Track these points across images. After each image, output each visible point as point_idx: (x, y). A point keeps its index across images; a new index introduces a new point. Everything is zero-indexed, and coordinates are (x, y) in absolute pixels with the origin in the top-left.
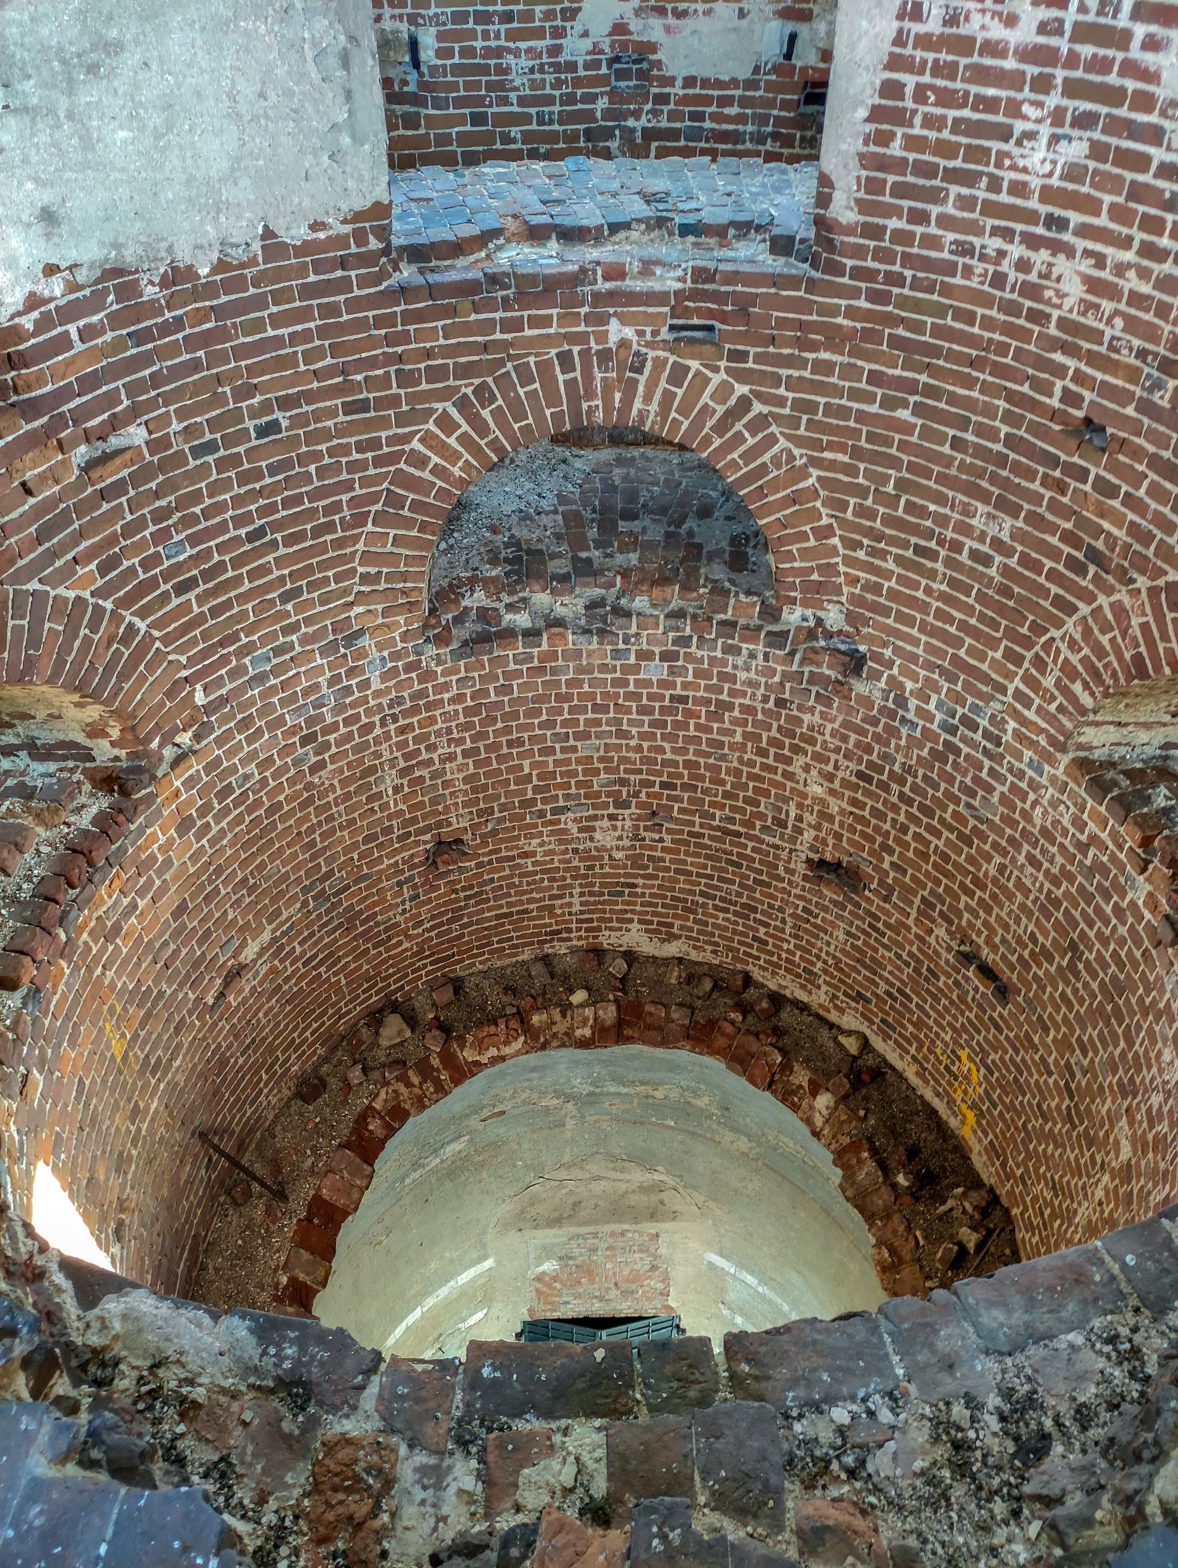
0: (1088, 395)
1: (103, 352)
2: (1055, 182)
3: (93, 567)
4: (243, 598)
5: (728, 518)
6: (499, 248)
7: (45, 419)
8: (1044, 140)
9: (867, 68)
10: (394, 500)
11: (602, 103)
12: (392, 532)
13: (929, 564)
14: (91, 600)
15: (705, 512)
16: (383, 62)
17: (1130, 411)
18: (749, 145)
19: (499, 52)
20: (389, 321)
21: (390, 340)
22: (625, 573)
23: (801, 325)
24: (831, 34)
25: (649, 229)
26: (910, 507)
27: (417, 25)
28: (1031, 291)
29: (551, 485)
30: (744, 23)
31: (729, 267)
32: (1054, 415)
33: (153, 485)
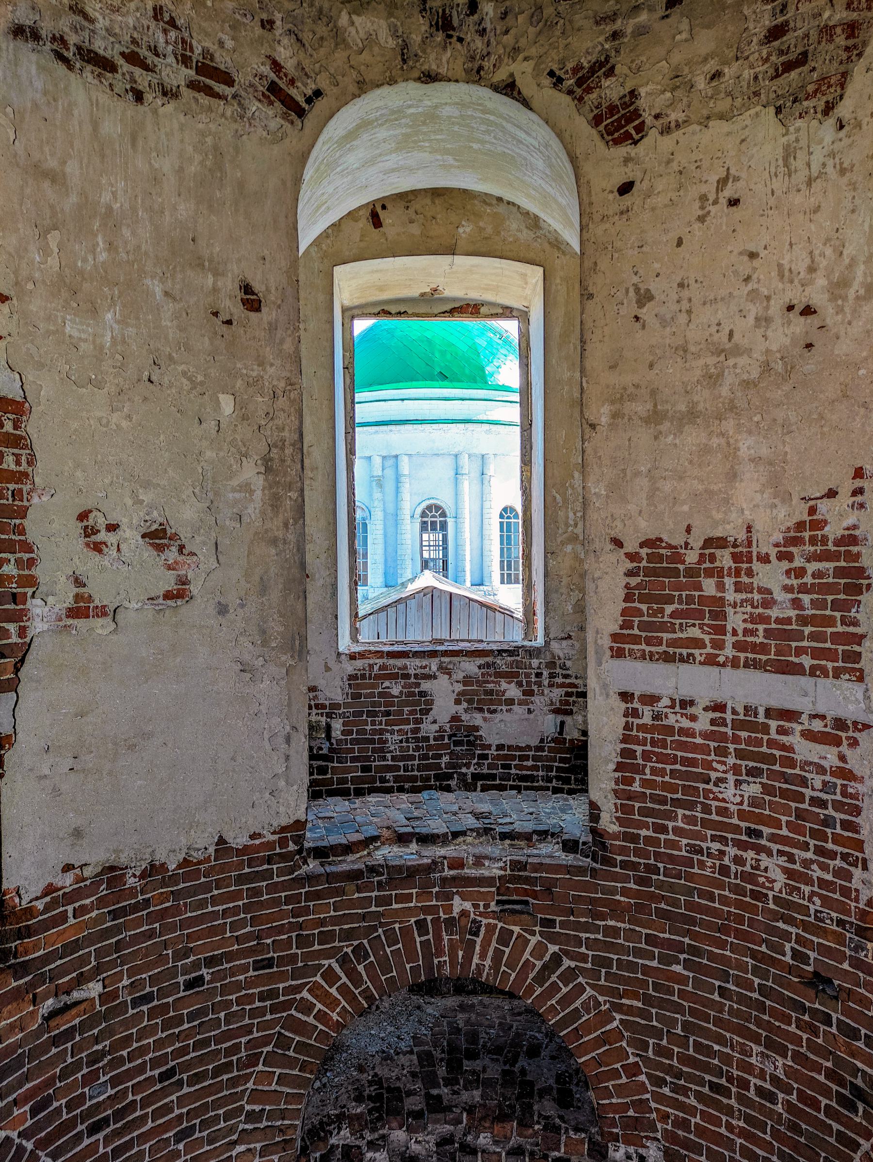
0: (812, 955)
1: (87, 925)
2: (745, 807)
3: (27, 1108)
4: (143, 1138)
5: (553, 1058)
6: (377, 848)
7: (31, 977)
8: (731, 783)
9: (610, 742)
10: (283, 1042)
11: (445, 759)
12: (278, 1071)
13: (725, 1101)
14: (17, 1141)
15: (534, 1051)
16: (311, 737)
17: (846, 966)
18: (541, 783)
19: (381, 732)
20: (296, 899)
21: (295, 914)
22: (470, 1110)
23: (592, 901)
24: (585, 722)
25: (479, 835)
26: (698, 1046)
27: (331, 718)
28: (750, 878)
29: (408, 1028)
30: (532, 716)
31: (535, 860)
32: (790, 969)
33: (96, 1031)
